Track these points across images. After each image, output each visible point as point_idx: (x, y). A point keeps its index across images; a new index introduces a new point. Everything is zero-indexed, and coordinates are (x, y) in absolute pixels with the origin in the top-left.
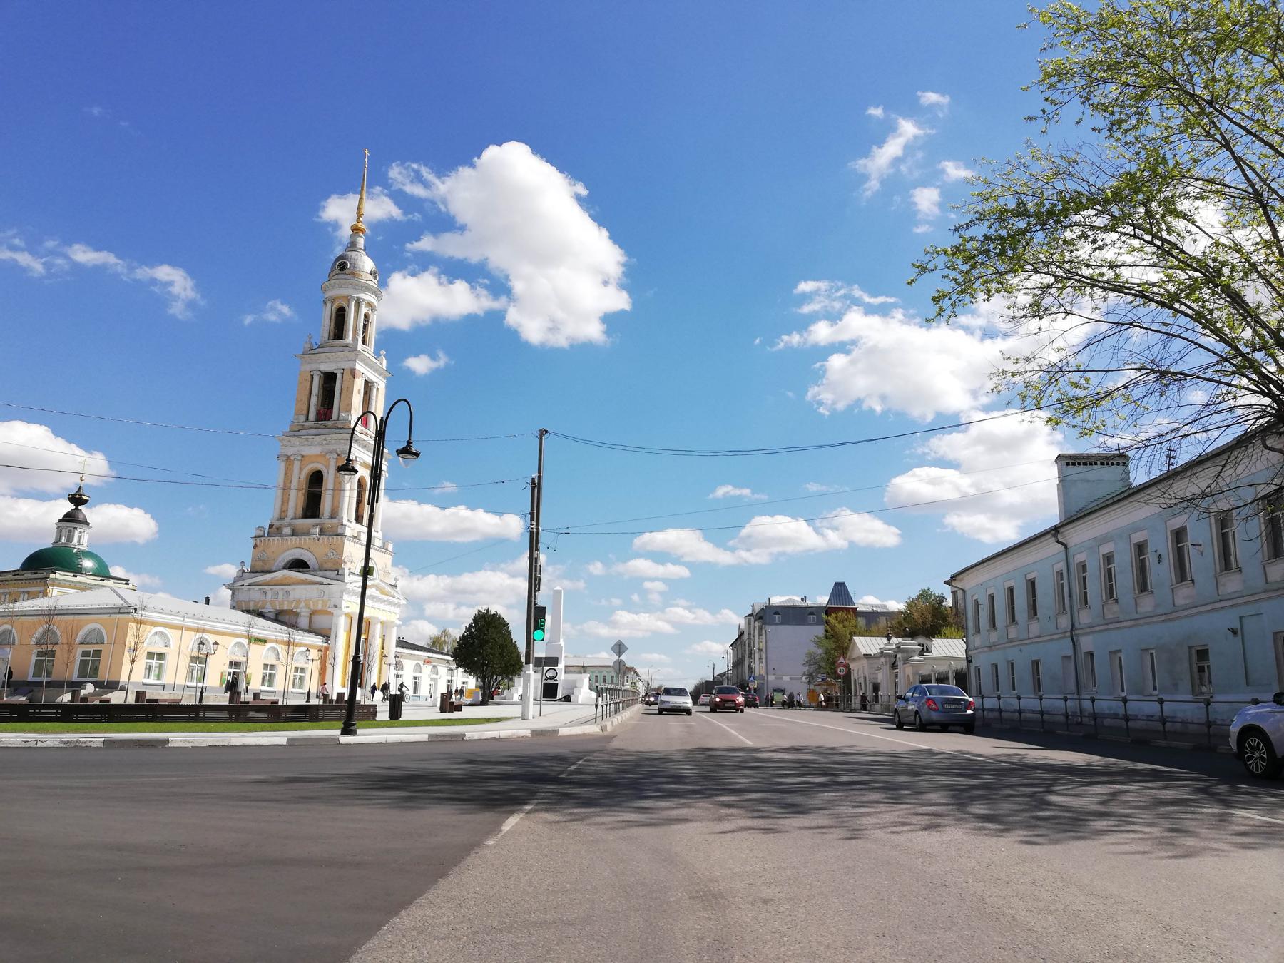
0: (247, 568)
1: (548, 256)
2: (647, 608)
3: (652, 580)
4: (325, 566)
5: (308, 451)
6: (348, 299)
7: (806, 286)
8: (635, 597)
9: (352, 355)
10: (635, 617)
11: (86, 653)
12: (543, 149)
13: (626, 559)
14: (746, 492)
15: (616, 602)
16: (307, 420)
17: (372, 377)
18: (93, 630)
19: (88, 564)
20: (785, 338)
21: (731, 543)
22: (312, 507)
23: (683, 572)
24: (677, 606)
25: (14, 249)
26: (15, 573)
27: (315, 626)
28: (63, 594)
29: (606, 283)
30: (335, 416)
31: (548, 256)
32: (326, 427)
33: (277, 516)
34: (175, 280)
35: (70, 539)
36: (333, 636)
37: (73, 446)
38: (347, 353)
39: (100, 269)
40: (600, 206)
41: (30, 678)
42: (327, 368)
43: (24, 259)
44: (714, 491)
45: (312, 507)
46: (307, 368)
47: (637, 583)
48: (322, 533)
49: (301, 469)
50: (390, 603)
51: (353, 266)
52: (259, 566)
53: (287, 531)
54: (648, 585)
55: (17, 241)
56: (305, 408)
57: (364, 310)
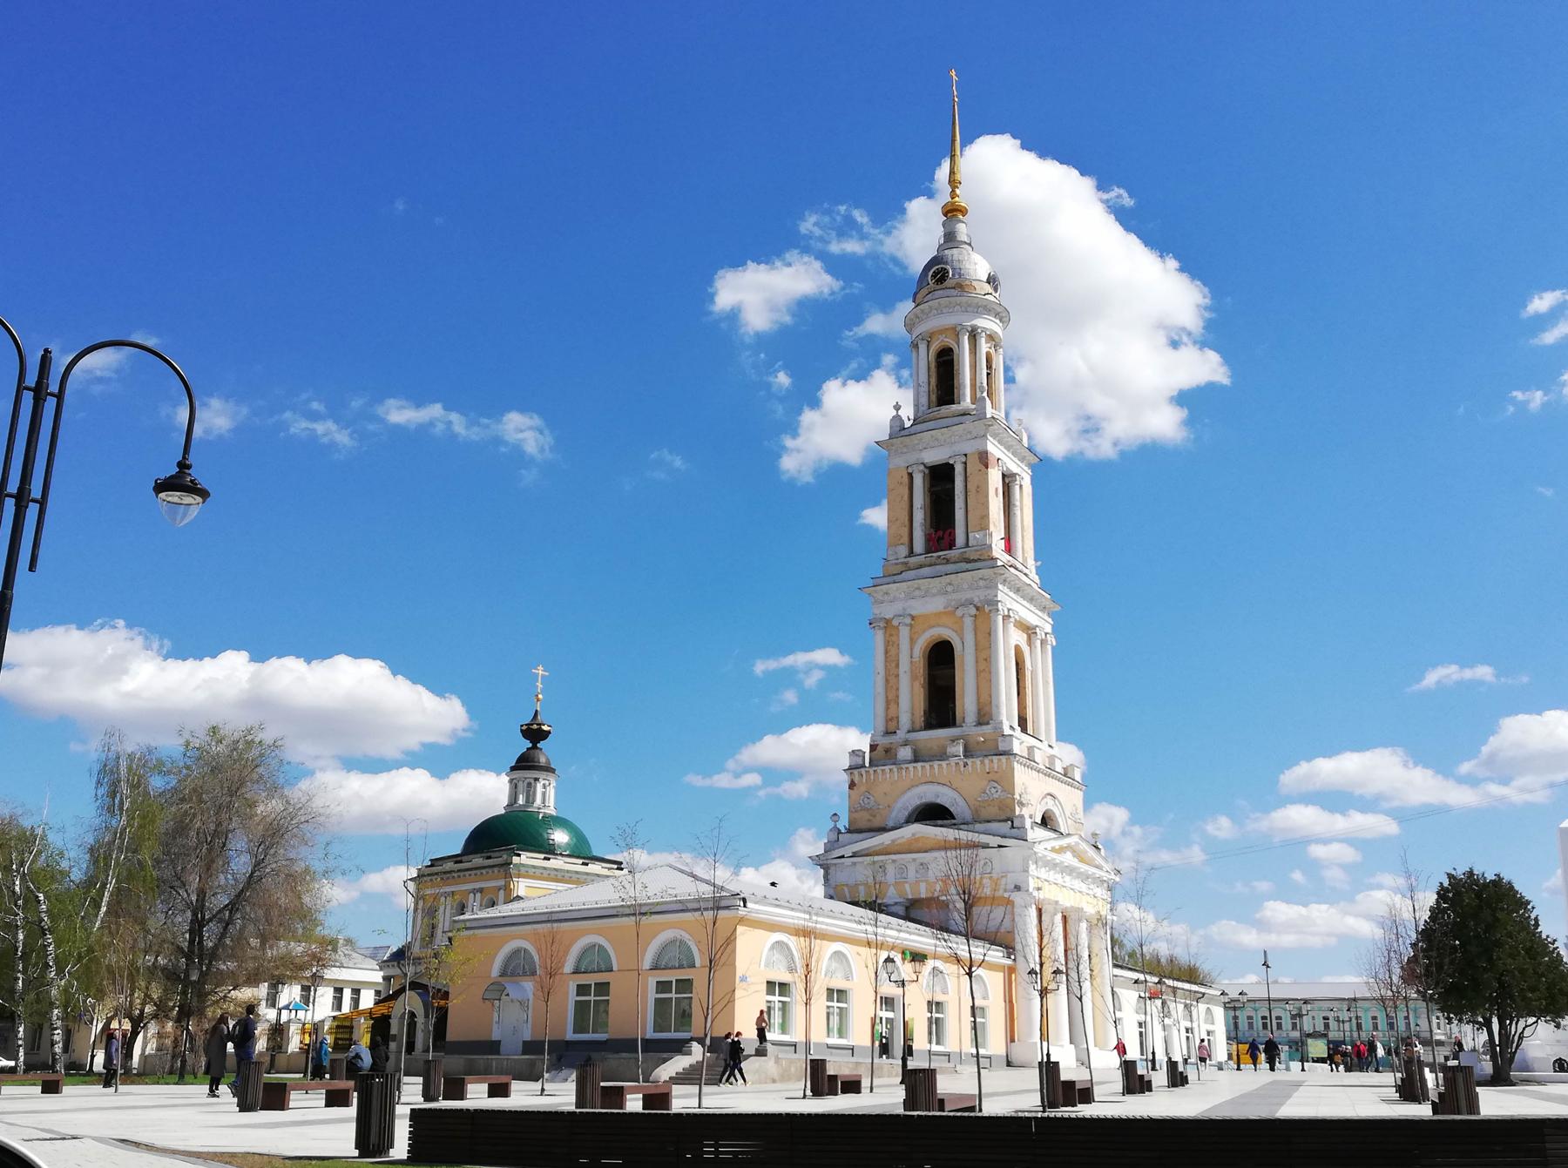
0: (843, 824)
1: (1074, 313)
2: (1318, 891)
3: (1326, 841)
4: (984, 814)
5: (919, 607)
6: (955, 332)
7: (1541, 303)
8: (1297, 876)
9: (977, 427)
10: (1303, 910)
11: (663, 986)
12: (1041, 143)
13: (1267, 809)
14: (1484, 672)
15: (1263, 886)
16: (911, 553)
17: (1013, 466)
18: (673, 942)
19: (560, 837)
20: (1518, 395)
21: (1465, 768)
22: (941, 705)
23: (1390, 827)
24: (1380, 887)
25: (314, 417)
26: (456, 858)
27: (980, 927)
28: (536, 888)
29: (1175, 344)
30: (960, 539)
31: (1074, 313)
32: (948, 561)
33: (881, 728)
34: (521, 429)
35: (530, 799)
36: (1018, 947)
37: (420, 688)
38: (969, 425)
39: (424, 429)
40: (1149, 222)
41: (570, 1035)
42: (935, 457)
43: (325, 429)
44: (1421, 678)
45: (941, 705)
46: (900, 462)
47: (1296, 845)
48: (968, 753)
49: (912, 641)
50: (1085, 877)
51: (959, 273)
52: (863, 820)
53: (905, 753)
54: (1318, 851)
55: (315, 405)
56: (906, 531)
57: (984, 347)
